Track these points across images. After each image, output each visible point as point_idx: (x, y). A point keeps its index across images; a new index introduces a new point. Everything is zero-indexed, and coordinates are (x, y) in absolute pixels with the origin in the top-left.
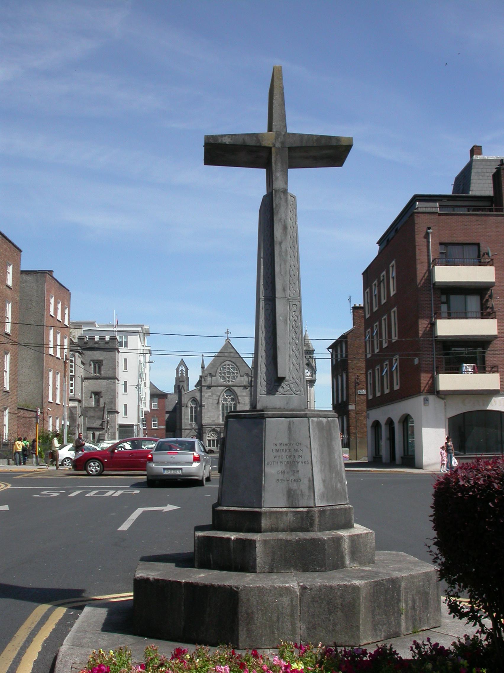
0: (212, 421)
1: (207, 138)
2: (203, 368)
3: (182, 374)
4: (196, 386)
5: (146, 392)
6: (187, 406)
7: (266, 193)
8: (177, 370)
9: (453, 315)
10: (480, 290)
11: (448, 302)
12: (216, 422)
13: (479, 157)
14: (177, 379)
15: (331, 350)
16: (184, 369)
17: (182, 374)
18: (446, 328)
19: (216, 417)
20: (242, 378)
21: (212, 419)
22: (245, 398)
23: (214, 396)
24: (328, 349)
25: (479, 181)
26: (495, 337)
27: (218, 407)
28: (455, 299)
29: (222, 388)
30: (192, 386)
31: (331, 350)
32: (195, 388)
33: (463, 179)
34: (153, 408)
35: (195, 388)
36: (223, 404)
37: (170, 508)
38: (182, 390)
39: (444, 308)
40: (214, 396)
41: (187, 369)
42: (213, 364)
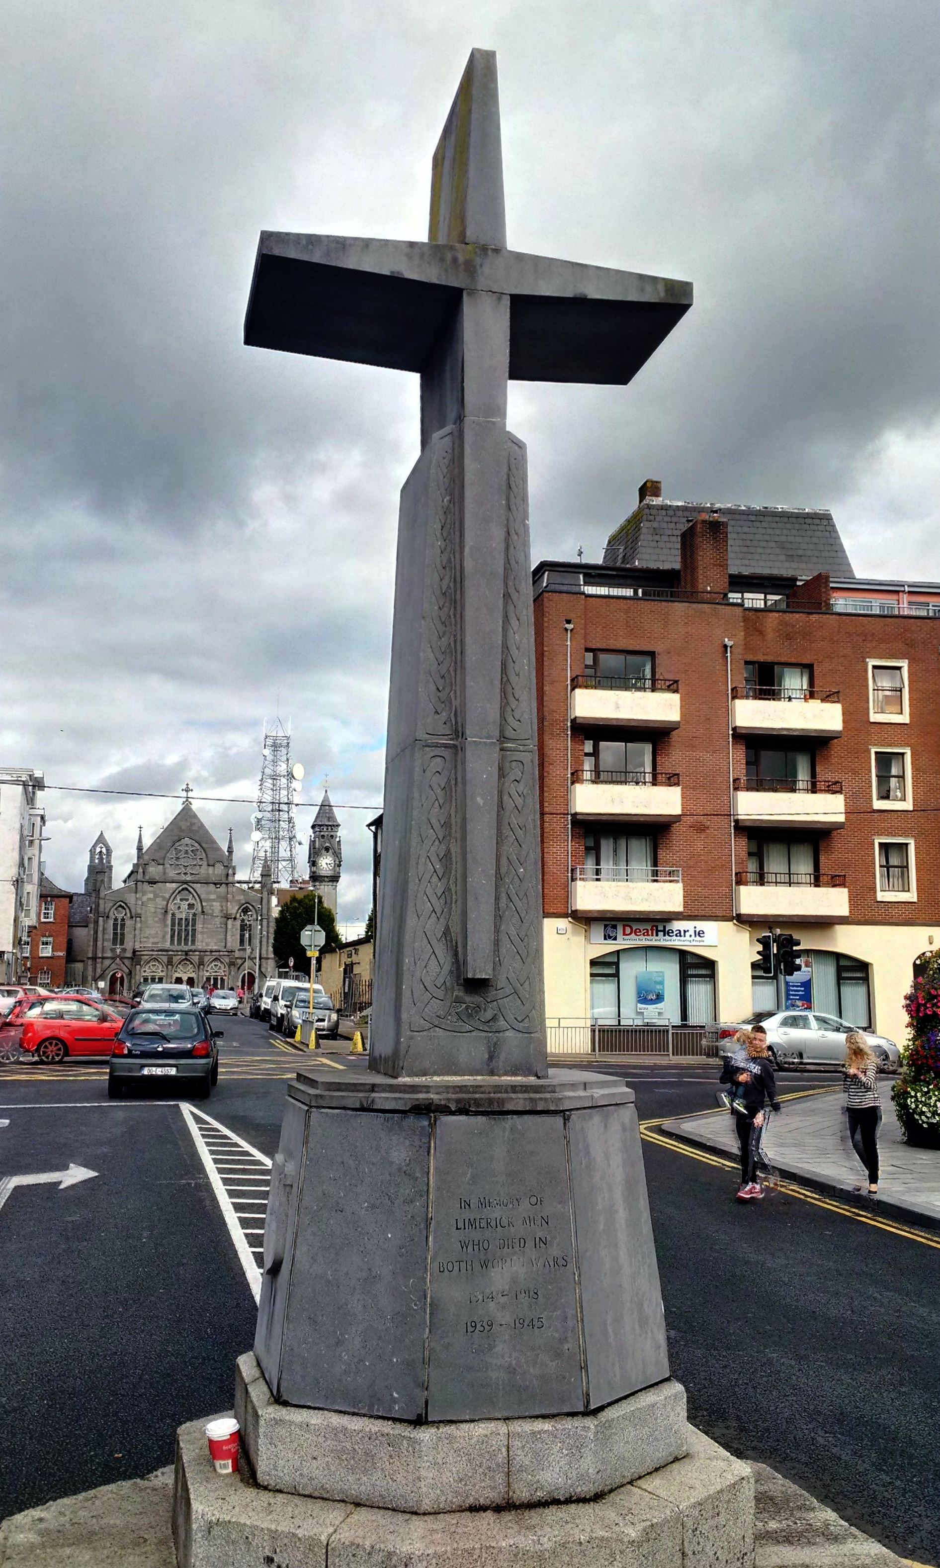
0: (153, 943)
1: (266, 237)
2: (140, 849)
3: (101, 859)
4: (125, 882)
5: (32, 888)
6: (108, 917)
7: (508, 429)
8: (92, 852)
9: (603, 776)
10: (655, 735)
11: (595, 754)
12: (160, 946)
13: (657, 501)
14: (91, 868)
15: (373, 828)
16: (104, 850)
17: (101, 859)
18: (592, 799)
19: (160, 936)
20: (211, 869)
21: (152, 940)
22: (214, 903)
23: (159, 900)
24: (369, 825)
25: (774, 525)
26: (677, 819)
27: (164, 920)
28: (611, 750)
29: (174, 885)
30: (117, 883)
31: (373, 828)
32: (123, 885)
33: (627, 536)
34: (43, 920)
35: (123, 885)
36: (173, 915)
37: (75, 1175)
38: (102, 888)
39: (588, 765)
40: (159, 900)
41: (109, 851)
42: (158, 844)
